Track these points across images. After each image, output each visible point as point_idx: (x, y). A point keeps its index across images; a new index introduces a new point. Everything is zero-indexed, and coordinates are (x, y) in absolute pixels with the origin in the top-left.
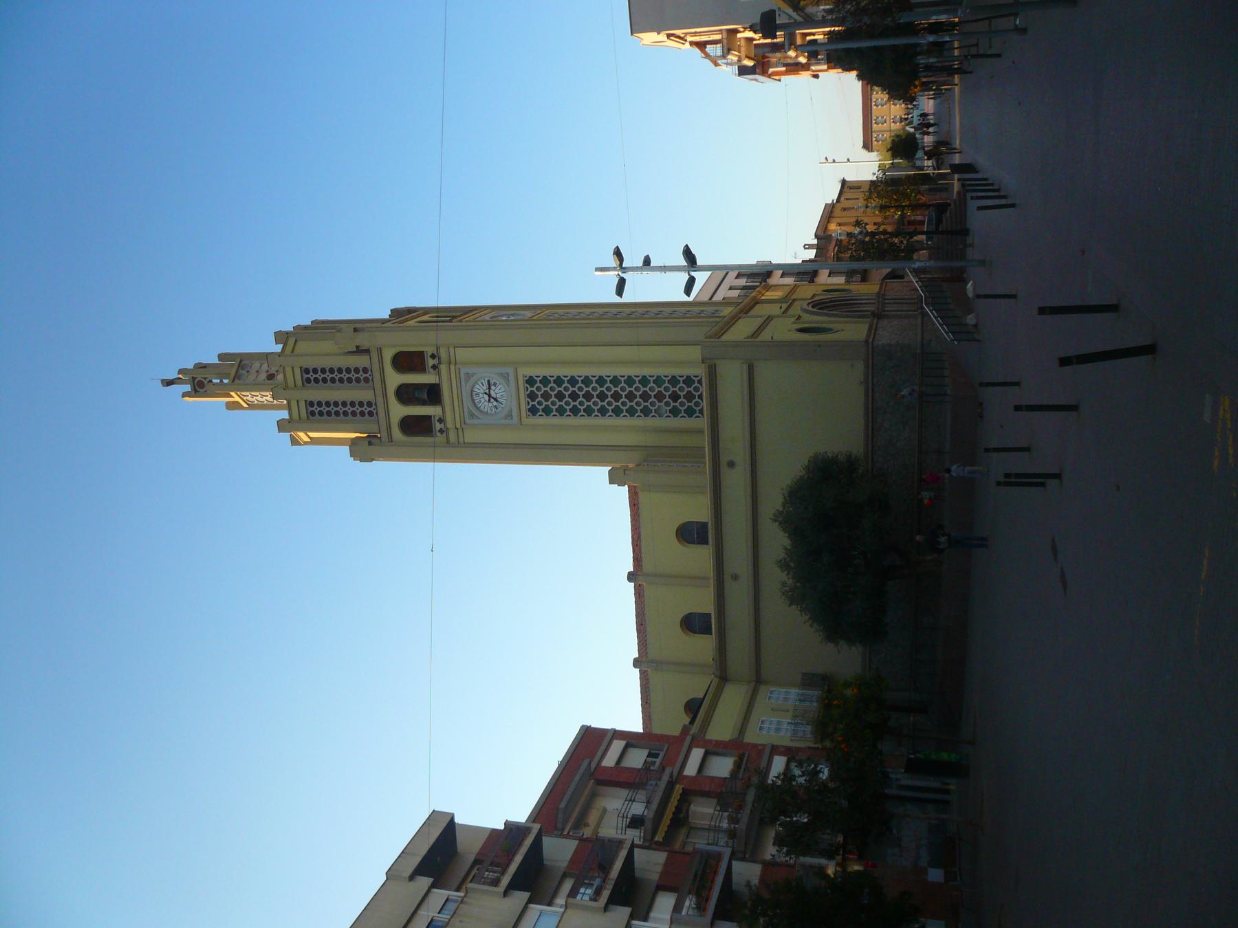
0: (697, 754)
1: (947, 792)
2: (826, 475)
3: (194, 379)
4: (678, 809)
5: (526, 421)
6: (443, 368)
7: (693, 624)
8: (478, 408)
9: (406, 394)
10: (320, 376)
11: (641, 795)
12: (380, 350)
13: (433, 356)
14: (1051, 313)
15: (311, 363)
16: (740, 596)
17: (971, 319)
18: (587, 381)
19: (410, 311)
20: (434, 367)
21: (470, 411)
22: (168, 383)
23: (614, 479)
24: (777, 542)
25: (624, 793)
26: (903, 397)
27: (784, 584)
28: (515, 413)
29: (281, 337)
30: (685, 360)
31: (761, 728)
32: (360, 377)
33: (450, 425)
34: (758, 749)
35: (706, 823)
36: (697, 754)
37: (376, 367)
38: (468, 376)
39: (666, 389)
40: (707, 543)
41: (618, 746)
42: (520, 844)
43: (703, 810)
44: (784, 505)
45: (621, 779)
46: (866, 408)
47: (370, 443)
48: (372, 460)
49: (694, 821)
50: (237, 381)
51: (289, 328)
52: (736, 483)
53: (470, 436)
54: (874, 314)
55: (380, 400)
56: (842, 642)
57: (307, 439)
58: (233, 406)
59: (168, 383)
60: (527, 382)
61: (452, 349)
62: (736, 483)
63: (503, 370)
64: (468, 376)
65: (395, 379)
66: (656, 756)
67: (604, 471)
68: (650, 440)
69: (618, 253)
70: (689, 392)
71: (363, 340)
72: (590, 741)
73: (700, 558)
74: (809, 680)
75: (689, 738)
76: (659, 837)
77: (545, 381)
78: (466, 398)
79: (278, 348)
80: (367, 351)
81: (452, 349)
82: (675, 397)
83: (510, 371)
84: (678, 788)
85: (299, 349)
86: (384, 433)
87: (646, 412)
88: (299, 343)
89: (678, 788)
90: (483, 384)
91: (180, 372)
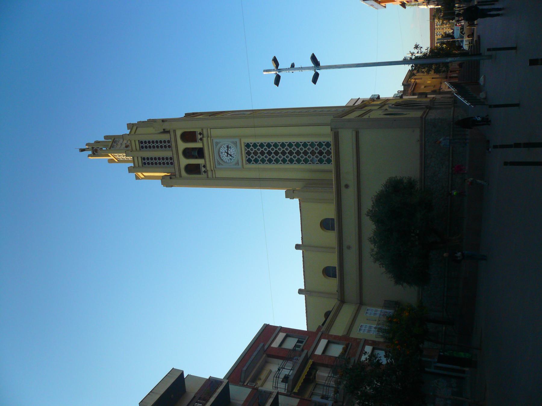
0: (323, 343)
1: (464, 372)
2: (396, 189)
3: (93, 148)
4: (309, 373)
5: (245, 166)
6: (205, 139)
7: (328, 272)
8: (222, 160)
9: (187, 153)
10: (148, 145)
11: (289, 365)
12: (175, 131)
13: (200, 134)
14: (520, 144)
15: (144, 138)
16: (351, 259)
17: (482, 95)
18: (276, 145)
19: (194, 114)
20: (201, 139)
21: (218, 161)
22: (82, 150)
23: (289, 195)
24: (370, 227)
25: (280, 361)
26: (440, 142)
27: (373, 250)
28: (240, 163)
29: (130, 126)
30: (324, 134)
31: (360, 330)
32: (166, 145)
33: (208, 168)
34: (357, 341)
35: (323, 382)
36: (323, 343)
37: (173, 140)
38: (217, 143)
39: (316, 149)
40: (334, 230)
41: (282, 335)
42: (215, 391)
43: (323, 374)
44: (373, 207)
45: (282, 355)
46: (421, 156)
47: (171, 178)
48: (172, 186)
49: (319, 380)
50: (112, 149)
51: (135, 122)
52: (349, 196)
53: (219, 174)
54: (427, 107)
55: (175, 156)
56: (405, 284)
57: (143, 177)
58: (111, 161)
59: (82, 150)
60: (246, 146)
61: (209, 130)
62: (349, 196)
63: (234, 140)
64: (217, 143)
65: (182, 146)
66: (302, 342)
67: (283, 192)
68: (307, 176)
69: (275, 60)
70: (262, 148)
71: (166, 126)
72: (268, 332)
73: (331, 237)
74: (388, 304)
75: (320, 334)
76: (296, 390)
77: (255, 145)
78: (217, 157)
79: (128, 132)
80: (168, 132)
81: (209, 130)
82: (321, 153)
83: (237, 140)
84: (311, 362)
85: (138, 132)
86: (177, 173)
87: (306, 161)
88: (138, 129)
89: (311, 362)
90: (225, 148)
91: (87, 145)
